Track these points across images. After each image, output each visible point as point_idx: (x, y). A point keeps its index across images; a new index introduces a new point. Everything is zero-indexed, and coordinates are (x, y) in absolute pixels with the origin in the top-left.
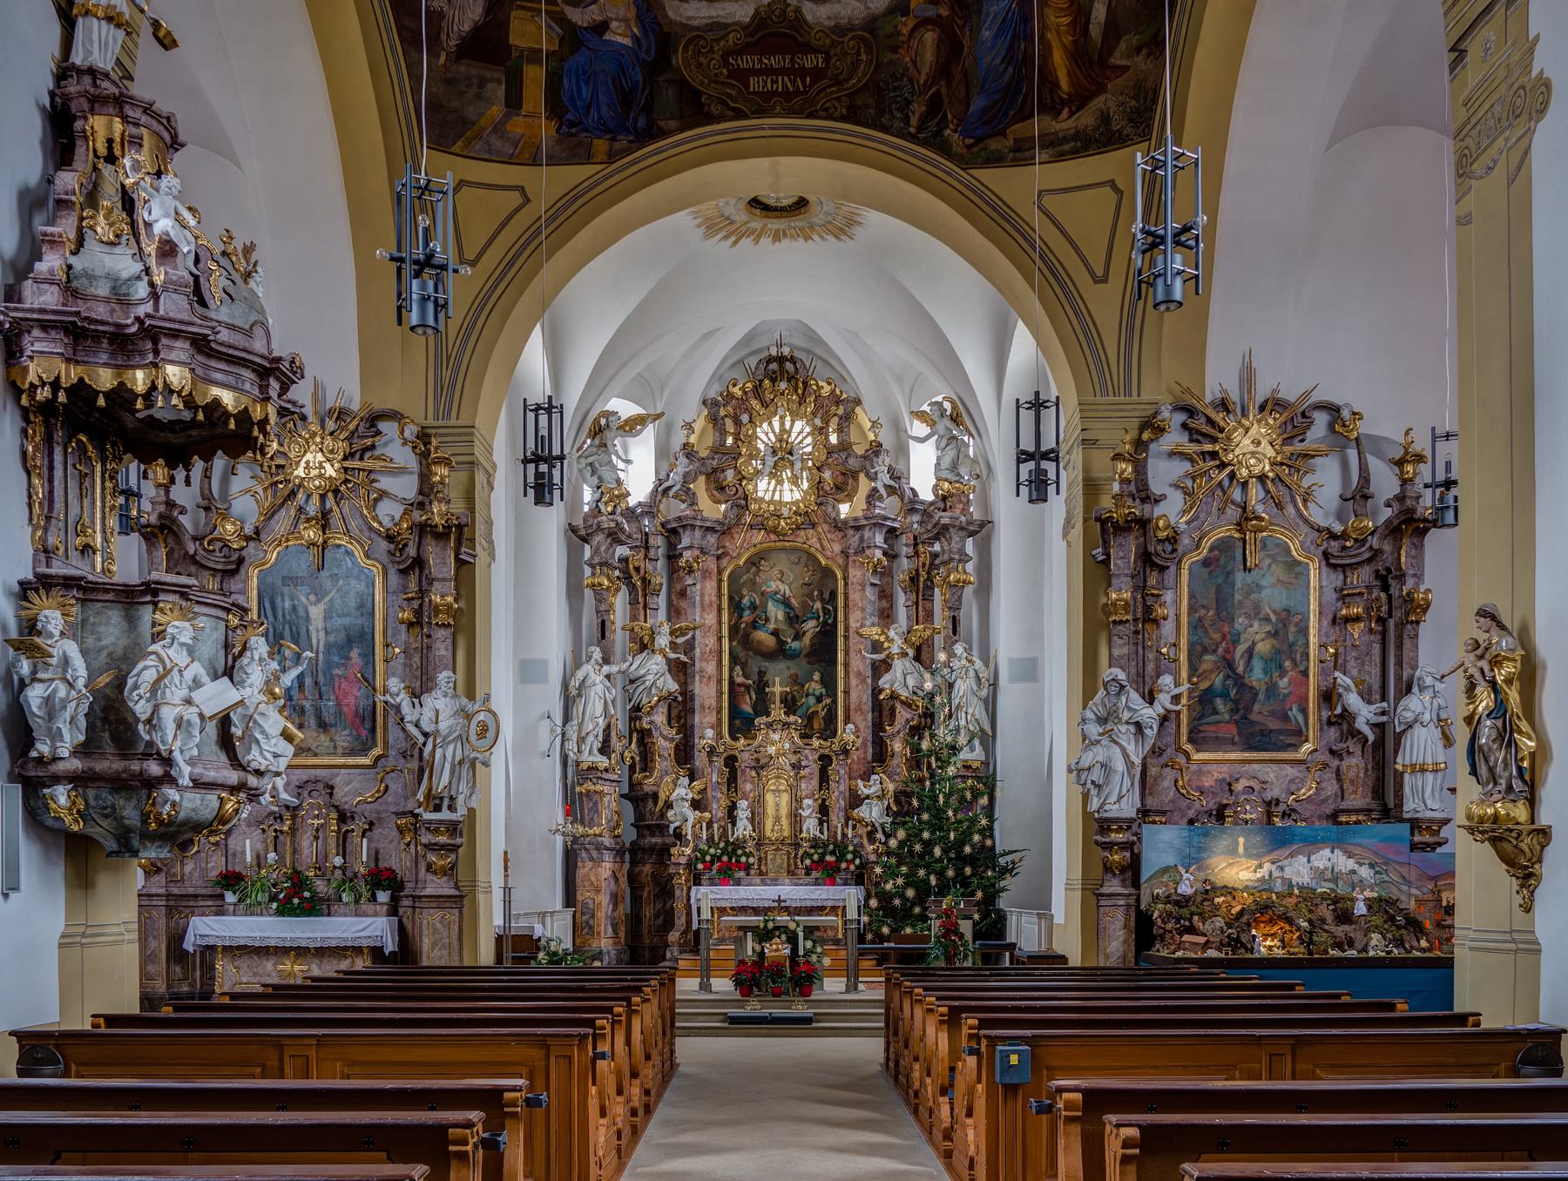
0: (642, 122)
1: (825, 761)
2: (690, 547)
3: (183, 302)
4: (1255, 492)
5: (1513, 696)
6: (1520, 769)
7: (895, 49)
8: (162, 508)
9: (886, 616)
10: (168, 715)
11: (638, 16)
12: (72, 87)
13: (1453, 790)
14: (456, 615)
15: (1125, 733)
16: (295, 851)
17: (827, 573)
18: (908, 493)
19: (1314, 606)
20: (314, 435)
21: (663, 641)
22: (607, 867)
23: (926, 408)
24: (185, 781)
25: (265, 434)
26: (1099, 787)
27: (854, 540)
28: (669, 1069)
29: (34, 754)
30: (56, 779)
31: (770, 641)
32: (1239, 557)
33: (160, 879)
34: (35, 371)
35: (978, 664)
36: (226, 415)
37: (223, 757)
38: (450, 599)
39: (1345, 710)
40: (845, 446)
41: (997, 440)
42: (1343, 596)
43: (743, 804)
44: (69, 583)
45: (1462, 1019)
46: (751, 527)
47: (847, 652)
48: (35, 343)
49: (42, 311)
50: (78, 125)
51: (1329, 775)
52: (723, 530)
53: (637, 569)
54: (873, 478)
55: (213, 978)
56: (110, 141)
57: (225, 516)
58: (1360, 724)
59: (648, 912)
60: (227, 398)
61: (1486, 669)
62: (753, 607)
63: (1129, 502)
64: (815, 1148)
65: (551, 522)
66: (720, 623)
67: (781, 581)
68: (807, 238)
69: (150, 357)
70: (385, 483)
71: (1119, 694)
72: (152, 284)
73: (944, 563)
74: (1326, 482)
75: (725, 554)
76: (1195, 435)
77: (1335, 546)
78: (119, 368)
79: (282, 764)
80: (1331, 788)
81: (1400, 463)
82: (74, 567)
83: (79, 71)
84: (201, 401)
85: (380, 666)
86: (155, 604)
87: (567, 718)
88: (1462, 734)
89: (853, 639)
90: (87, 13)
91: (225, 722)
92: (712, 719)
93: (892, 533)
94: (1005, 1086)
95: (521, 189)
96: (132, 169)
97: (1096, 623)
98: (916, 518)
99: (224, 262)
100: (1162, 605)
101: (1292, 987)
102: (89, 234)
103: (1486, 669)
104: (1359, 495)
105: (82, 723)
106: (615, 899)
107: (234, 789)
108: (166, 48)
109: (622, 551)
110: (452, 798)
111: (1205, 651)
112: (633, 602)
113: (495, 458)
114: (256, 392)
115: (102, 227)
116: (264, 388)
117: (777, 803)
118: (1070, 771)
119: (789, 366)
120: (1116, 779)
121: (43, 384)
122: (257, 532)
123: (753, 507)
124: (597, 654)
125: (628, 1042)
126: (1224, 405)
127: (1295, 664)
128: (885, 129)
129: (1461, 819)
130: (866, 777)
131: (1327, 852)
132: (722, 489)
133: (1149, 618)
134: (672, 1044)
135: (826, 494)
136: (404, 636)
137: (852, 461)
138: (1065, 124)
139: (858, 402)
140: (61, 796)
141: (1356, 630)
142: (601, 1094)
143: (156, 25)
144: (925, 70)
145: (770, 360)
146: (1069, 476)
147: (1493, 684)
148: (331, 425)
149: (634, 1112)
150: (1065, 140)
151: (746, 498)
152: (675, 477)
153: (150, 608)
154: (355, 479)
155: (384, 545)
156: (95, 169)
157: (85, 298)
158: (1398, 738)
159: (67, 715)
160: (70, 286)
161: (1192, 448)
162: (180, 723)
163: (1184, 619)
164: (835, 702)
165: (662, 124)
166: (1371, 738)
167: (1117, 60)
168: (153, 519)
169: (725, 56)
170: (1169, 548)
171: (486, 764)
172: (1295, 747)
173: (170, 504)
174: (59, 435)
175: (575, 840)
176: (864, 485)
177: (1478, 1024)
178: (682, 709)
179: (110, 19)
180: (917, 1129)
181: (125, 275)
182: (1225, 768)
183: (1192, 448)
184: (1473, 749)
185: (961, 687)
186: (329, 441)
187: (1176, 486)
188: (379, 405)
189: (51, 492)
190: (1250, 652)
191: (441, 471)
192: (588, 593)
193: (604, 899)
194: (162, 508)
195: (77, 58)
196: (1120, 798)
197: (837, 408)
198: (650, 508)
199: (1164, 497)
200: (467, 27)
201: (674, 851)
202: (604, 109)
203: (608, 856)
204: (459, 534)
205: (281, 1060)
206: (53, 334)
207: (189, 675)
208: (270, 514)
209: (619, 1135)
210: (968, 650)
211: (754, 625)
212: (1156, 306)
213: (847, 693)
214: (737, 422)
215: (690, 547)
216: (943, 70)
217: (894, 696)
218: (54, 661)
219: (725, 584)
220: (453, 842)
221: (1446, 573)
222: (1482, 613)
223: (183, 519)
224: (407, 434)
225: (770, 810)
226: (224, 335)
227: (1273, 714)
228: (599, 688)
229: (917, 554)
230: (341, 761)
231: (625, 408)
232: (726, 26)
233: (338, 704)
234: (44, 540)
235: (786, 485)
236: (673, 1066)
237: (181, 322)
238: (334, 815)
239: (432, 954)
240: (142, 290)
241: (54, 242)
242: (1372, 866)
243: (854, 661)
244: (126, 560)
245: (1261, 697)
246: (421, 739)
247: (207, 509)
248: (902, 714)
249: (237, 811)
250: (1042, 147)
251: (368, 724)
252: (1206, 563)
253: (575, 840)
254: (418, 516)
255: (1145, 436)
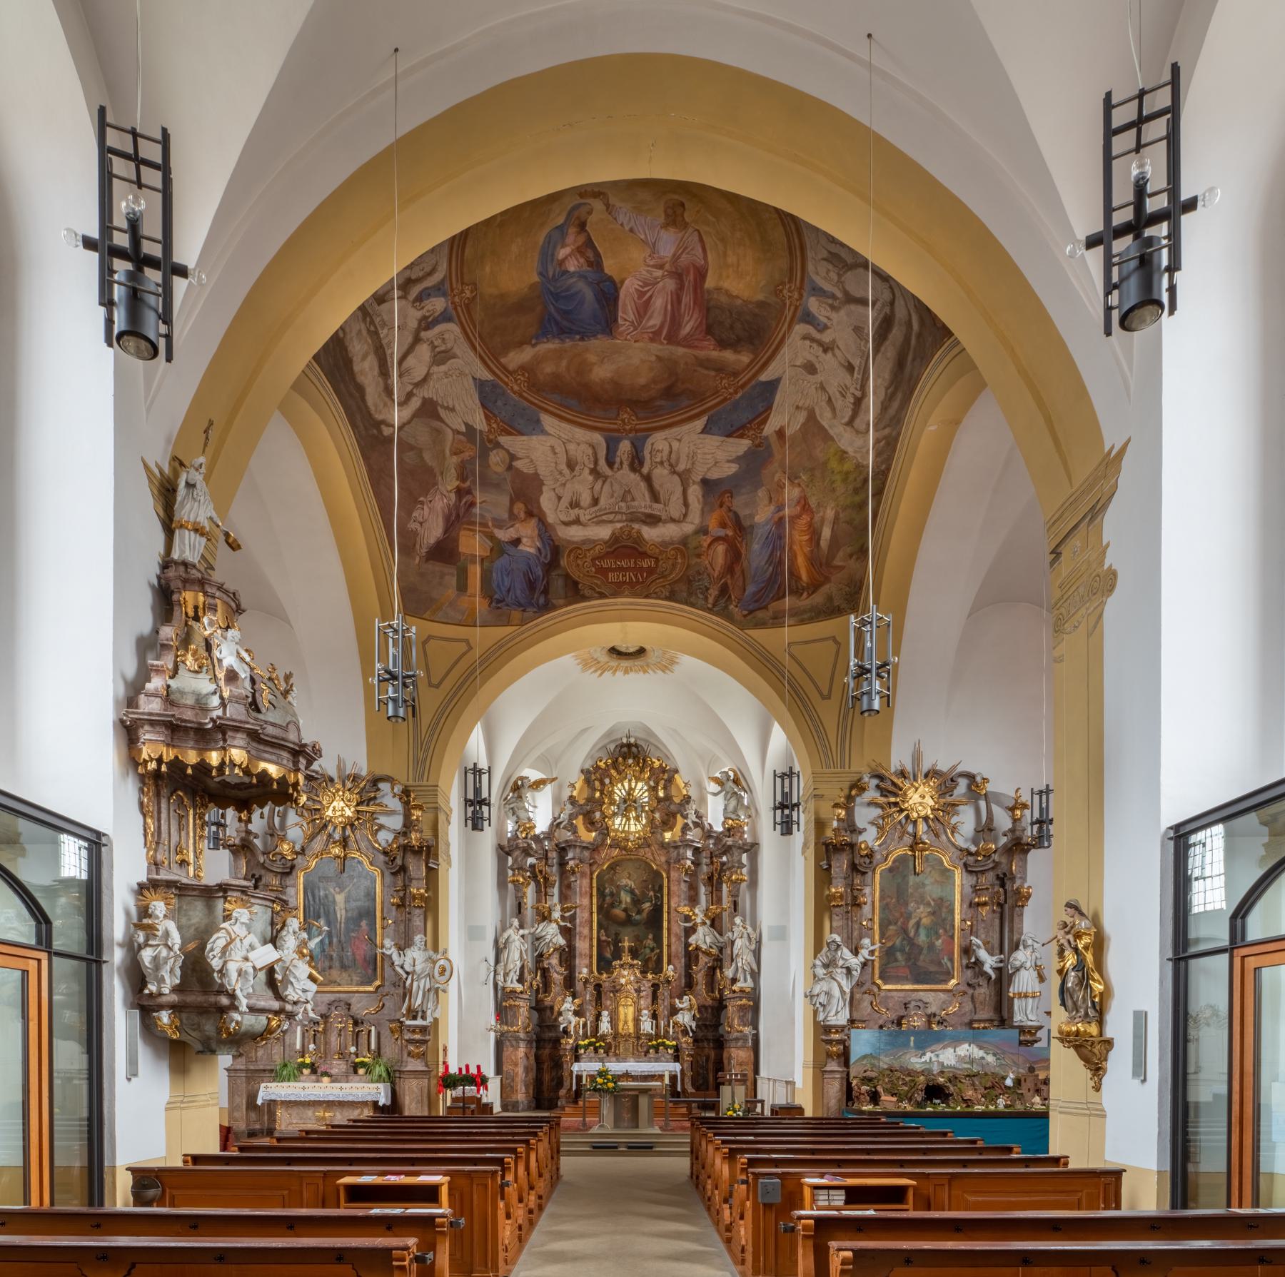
0: (542, 601)
1: (655, 987)
2: (573, 859)
3: (242, 709)
4: (922, 827)
5: (1089, 957)
6: (1093, 1003)
7: (699, 556)
8: (243, 835)
9: (693, 900)
10: (232, 968)
11: (539, 535)
12: (171, 573)
13: (1049, 1013)
14: (426, 900)
15: (840, 975)
16: (326, 1043)
17: (657, 875)
18: (707, 826)
19: (957, 897)
20: (338, 790)
21: (556, 915)
22: (522, 1051)
23: (718, 775)
24: (244, 1008)
25: (298, 792)
26: (824, 1006)
27: (674, 854)
28: (556, 1177)
29: (146, 991)
30: (161, 1007)
31: (622, 915)
32: (911, 866)
33: (242, 1060)
34: (146, 752)
35: (750, 930)
36: (272, 779)
37: (270, 993)
38: (422, 891)
39: (977, 959)
40: (668, 798)
41: (763, 794)
42: (976, 890)
43: (605, 1013)
44: (169, 884)
45: (1056, 1161)
46: (611, 846)
47: (669, 922)
48: (146, 734)
49: (150, 714)
50: (175, 597)
51: (967, 999)
52: (594, 848)
53: (541, 872)
54: (685, 817)
55: (275, 1120)
56: (196, 608)
57: (283, 839)
58: (987, 968)
59: (546, 1077)
60: (273, 770)
61: (1072, 940)
62: (612, 894)
63: (843, 833)
64: (644, 1234)
65: (488, 839)
66: (591, 904)
67: (628, 881)
68: (645, 672)
69: (221, 743)
70: (382, 820)
71: (836, 950)
72: (222, 698)
73: (729, 869)
74: (966, 821)
75: (595, 863)
76: (884, 792)
77: (971, 859)
78: (202, 751)
79: (310, 996)
80: (968, 1007)
81: (1012, 809)
82: (174, 874)
83: (176, 563)
84: (255, 771)
85: (379, 931)
86: (225, 898)
87: (497, 961)
88: (1055, 981)
89: (673, 914)
90: (181, 526)
91: (270, 971)
92: (587, 961)
93: (697, 851)
94: (765, 1205)
95: (467, 641)
96: (208, 626)
97: (823, 906)
98: (711, 841)
99: (269, 684)
100: (864, 895)
101: (945, 1134)
102: (181, 666)
103: (1072, 940)
104: (985, 829)
105: (178, 972)
106: (527, 1069)
107: (277, 1013)
108: (233, 549)
109: (531, 860)
110: (424, 1012)
111: (890, 923)
112: (538, 892)
113: (451, 805)
114: (291, 765)
115: (190, 660)
116: (296, 763)
117: (627, 1012)
118: (806, 996)
119: (634, 749)
120: (834, 1001)
121: (152, 760)
122: (303, 849)
123: (612, 834)
124: (516, 923)
125: (527, 1168)
126: (903, 774)
127: (946, 931)
128: (693, 605)
129: (1055, 1033)
130: (680, 998)
131: (966, 1046)
132: (592, 823)
133: (857, 904)
134: (558, 1164)
135: (657, 827)
136: (394, 913)
137: (672, 807)
138: (805, 602)
139: (676, 771)
140: (165, 1017)
141: (984, 911)
142: (507, 1206)
143: (227, 535)
144: (718, 569)
145: (622, 746)
146: (803, 818)
147: (1076, 950)
148: (349, 785)
149: (531, 1212)
150: (805, 612)
151: (607, 828)
152: (564, 816)
153: (222, 900)
154: (364, 819)
155: (382, 857)
156: (186, 624)
157: (178, 706)
158: (1011, 977)
159: (168, 968)
160: (169, 697)
161: (882, 800)
162: (240, 973)
163: (877, 904)
164: (662, 952)
165: (554, 601)
166: (993, 977)
167: (837, 562)
168: (237, 842)
169: (593, 560)
170: (868, 861)
171: (444, 991)
172: (946, 981)
173: (248, 832)
174: (165, 792)
175: (502, 1034)
176: (680, 821)
177: (1066, 1164)
178: (567, 956)
179: (196, 530)
180: (709, 1222)
181: (204, 691)
182: (902, 994)
183: (882, 800)
184: (1063, 990)
185: (739, 943)
186: (347, 794)
187: (872, 823)
188: (379, 772)
189: (159, 827)
190: (918, 924)
191: (417, 813)
192: (510, 886)
193: (520, 1070)
194: (243, 835)
195: (175, 555)
196: (837, 1013)
197: (665, 775)
198: (549, 835)
199: (865, 830)
200: (432, 541)
201: (563, 1041)
202: (518, 592)
203: (522, 1044)
204: (429, 852)
205: (301, 1185)
206: (158, 728)
207: (246, 942)
208: (312, 838)
209: (520, 1228)
210: (744, 921)
211: (612, 905)
212: (862, 713)
213: (669, 946)
214: (602, 783)
215: (573, 859)
216: (729, 569)
217: (698, 948)
218: (159, 933)
219: (595, 881)
220: (424, 1039)
221: (1037, 871)
222: (1069, 905)
223: (257, 842)
224: (396, 790)
225: (622, 1017)
226: (270, 730)
227: (932, 962)
228: (517, 943)
229: (712, 863)
230: (355, 988)
231: (534, 775)
232: (594, 541)
233: (354, 954)
234: (154, 857)
235: (632, 822)
236: (558, 1177)
237: (241, 722)
238: (351, 1021)
239: (412, 1107)
240: (215, 701)
241: (159, 671)
242: (994, 1055)
243: (671, 928)
244: (216, 867)
245: (925, 951)
246: (405, 976)
247: (272, 835)
248: (703, 959)
249: (279, 1026)
250: (791, 616)
251: (372, 966)
252: (891, 870)
253: (502, 1034)
254: (402, 841)
255: (853, 793)
